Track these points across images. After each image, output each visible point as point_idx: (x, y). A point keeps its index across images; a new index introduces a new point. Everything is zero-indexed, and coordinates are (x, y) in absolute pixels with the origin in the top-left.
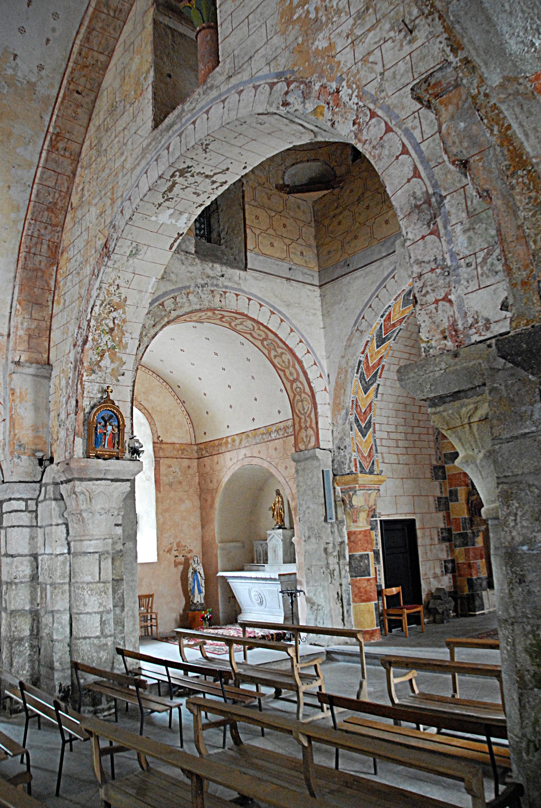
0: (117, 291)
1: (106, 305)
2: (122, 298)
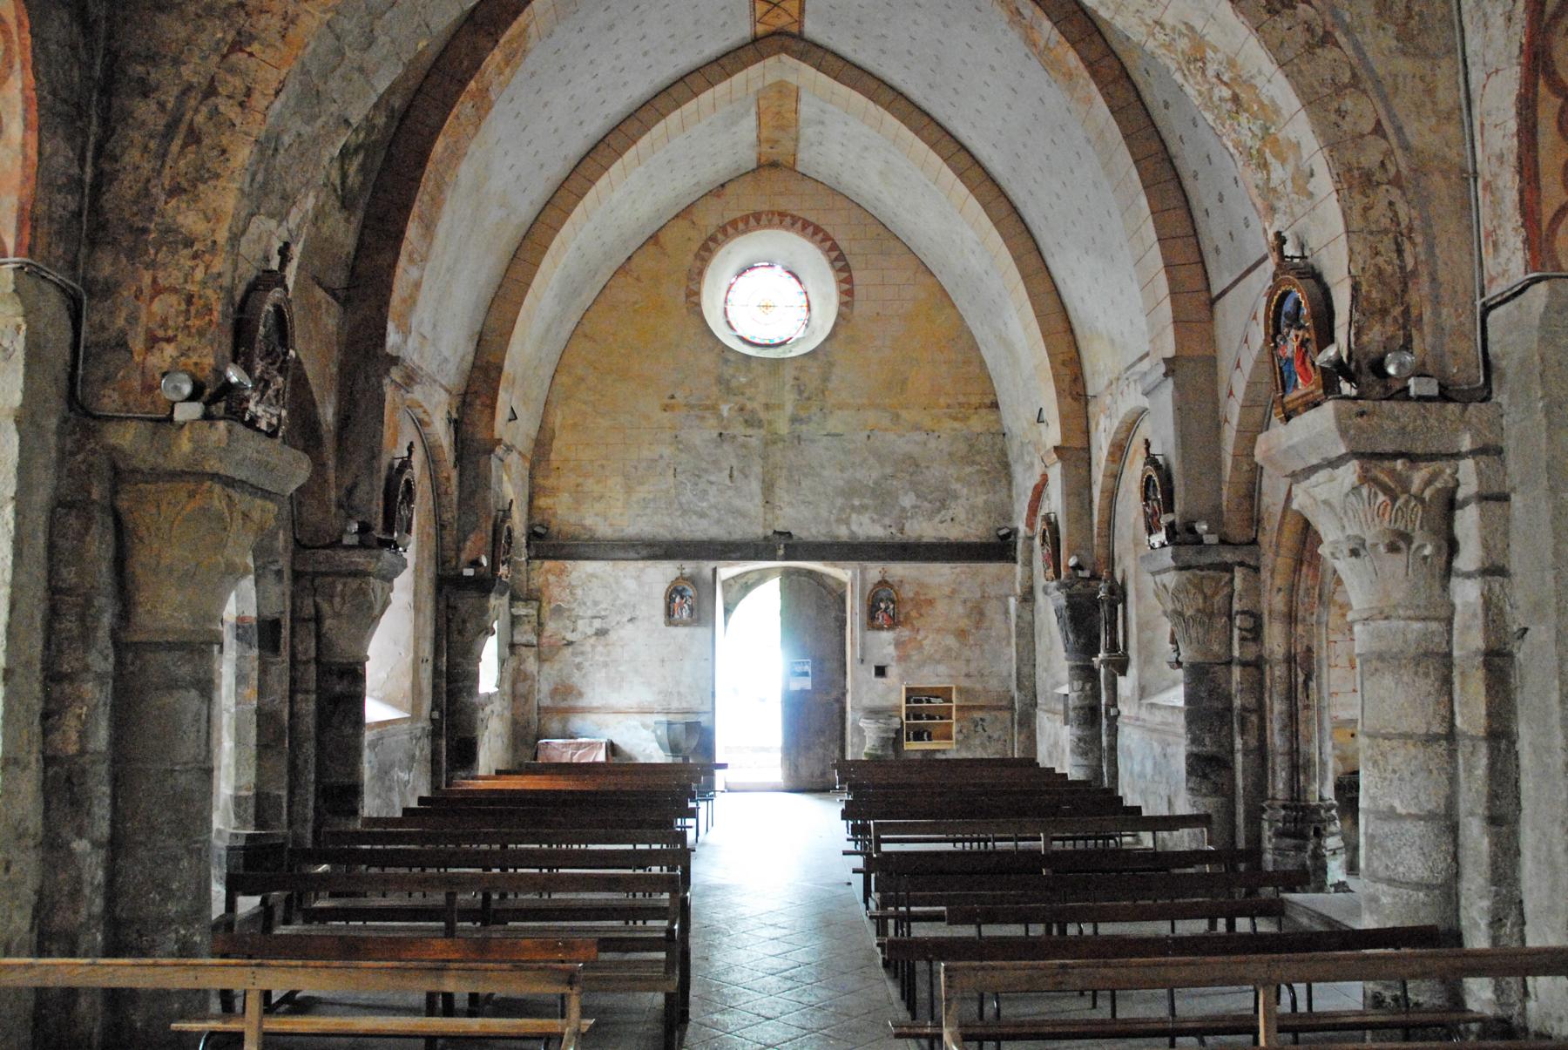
0: (1168, 31)
1: (1189, 70)
2: (1185, 31)
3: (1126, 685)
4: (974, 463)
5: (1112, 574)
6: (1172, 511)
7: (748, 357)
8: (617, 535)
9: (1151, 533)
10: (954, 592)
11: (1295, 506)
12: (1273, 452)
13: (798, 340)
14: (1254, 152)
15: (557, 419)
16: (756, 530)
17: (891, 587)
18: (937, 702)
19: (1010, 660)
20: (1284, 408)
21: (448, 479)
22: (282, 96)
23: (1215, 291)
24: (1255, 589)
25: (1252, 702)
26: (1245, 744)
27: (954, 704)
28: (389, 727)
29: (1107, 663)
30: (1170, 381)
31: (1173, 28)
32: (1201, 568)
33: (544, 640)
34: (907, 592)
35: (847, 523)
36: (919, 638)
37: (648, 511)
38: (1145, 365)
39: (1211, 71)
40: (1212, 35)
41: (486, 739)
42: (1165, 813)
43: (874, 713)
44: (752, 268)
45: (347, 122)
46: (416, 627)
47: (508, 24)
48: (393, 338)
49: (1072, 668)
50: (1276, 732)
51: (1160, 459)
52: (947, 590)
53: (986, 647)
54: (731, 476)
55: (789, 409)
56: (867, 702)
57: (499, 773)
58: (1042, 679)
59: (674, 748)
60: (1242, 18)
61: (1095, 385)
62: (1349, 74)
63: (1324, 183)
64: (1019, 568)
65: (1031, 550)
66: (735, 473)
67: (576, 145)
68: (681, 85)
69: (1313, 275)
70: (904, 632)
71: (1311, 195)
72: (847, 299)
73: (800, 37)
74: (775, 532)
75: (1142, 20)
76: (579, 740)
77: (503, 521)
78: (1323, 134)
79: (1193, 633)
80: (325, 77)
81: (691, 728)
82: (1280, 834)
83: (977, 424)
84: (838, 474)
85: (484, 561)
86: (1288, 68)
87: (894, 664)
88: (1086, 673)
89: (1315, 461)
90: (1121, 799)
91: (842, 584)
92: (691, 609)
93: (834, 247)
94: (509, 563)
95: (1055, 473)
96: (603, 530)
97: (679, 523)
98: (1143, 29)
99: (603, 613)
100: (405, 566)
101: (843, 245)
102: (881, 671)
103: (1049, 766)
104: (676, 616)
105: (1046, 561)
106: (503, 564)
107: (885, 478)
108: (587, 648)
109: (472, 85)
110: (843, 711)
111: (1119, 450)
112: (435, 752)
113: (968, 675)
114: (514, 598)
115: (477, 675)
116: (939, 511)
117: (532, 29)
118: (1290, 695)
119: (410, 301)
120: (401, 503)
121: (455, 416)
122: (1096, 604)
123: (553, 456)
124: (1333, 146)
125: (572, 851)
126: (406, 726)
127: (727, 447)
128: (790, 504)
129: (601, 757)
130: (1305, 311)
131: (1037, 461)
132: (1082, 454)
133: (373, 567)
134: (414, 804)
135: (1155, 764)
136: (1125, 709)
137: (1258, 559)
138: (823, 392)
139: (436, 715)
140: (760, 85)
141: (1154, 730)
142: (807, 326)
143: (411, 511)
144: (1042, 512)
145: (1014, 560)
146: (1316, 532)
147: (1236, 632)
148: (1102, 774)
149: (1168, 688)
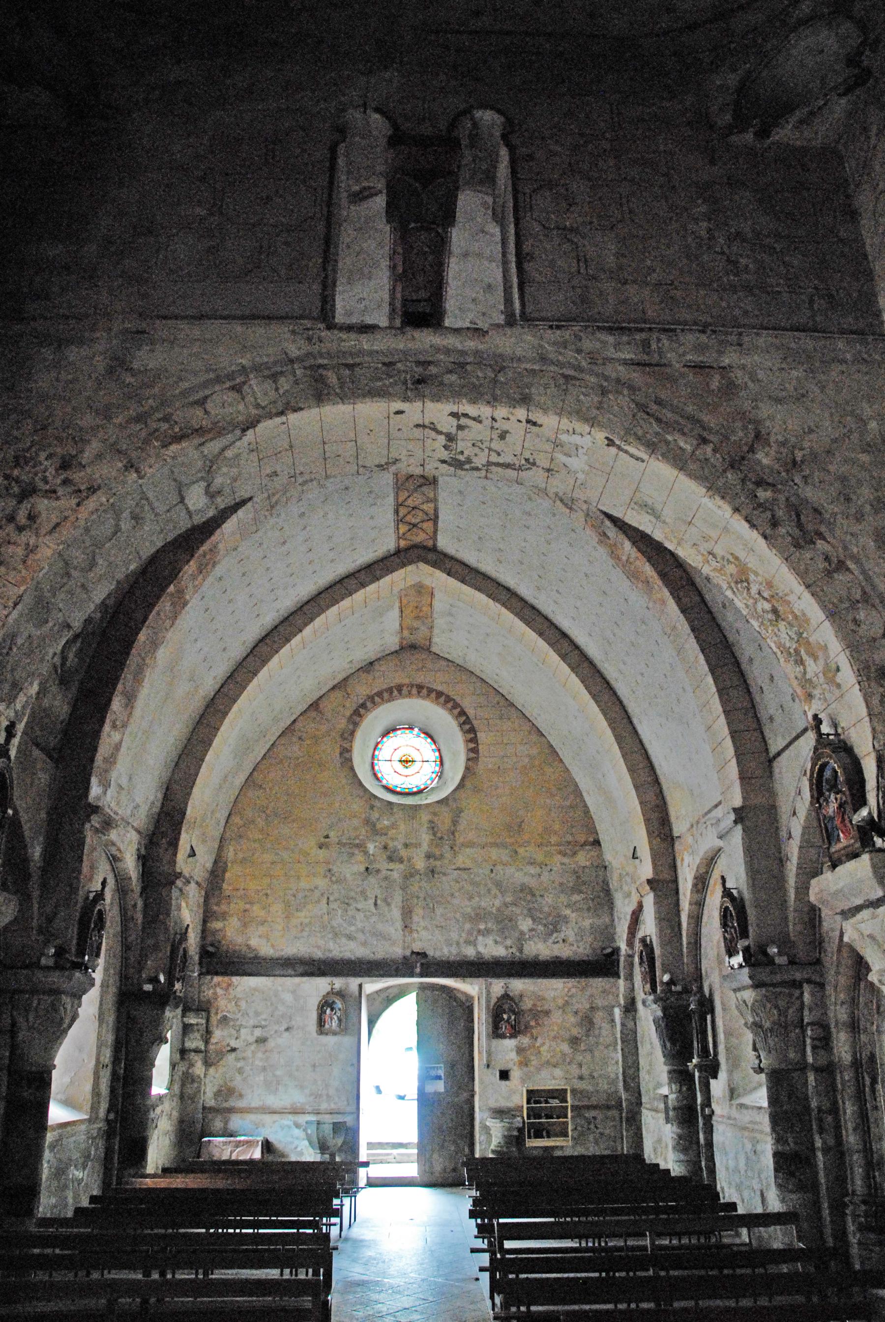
3: (718, 1087)
4: (581, 892)
5: (701, 988)
6: (747, 937)
7: (390, 803)
8: (277, 955)
9: (730, 956)
10: (567, 1003)
11: (846, 939)
12: (825, 893)
13: (433, 789)
14: (792, 651)
15: (230, 853)
16: (397, 951)
17: (512, 999)
18: (555, 1103)
19: (617, 1063)
20: (830, 857)
21: (135, 906)
22: (19, 607)
23: (773, 750)
24: (821, 1004)
25: (826, 1105)
26: (824, 1143)
27: (569, 1104)
28: (69, 1129)
29: (699, 1067)
30: (739, 827)
31: (723, 558)
32: (774, 985)
33: (211, 1047)
34: (527, 1004)
35: (474, 944)
36: (538, 1044)
37: (305, 934)
38: (719, 812)
39: (754, 590)
40: (752, 563)
41: (155, 1137)
42: (759, 1210)
43: (500, 1113)
44: (395, 730)
45: (69, 627)
46: (99, 1035)
47: (202, 542)
48: (95, 790)
49: (670, 1072)
50: (850, 1131)
51: (735, 892)
52: (560, 1002)
53: (597, 1054)
54: (376, 904)
55: (425, 847)
56: (493, 1104)
57: (166, 1171)
58: (645, 1080)
59: (323, 1147)
60: (774, 551)
61: (679, 827)
62: (859, 591)
63: (848, 676)
64: (621, 982)
65: (632, 965)
66: (379, 902)
67: (253, 632)
68: (339, 586)
69: (844, 749)
70: (525, 1040)
71: (839, 686)
72: (472, 755)
73: (434, 549)
74: (413, 953)
75: (699, 552)
76: (238, 1138)
77: (180, 943)
78: (844, 639)
79: (771, 1042)
80: (54, 592)
81: (337, 1127)
82: (861, 1228)
83: (583, 858)
84: (468, 903)
85: (162, 978)
86: (813, 588)
87: (515, 1068)
88: (682, 1077)
89: (859, 902)
90: (717, 1195)
91: (470, 998)
92: (340, 1020)
93: (463, 713)
94: (183, 980)
95: (649, 901)
96: (266, 950)
97: (331, 945)
98: (700, 558)
99: (263, 1023)
100: (93, 985)
101: (471, 712)
102: (504, 1075)
103: (654, 1162)
104: (327, 1026)
105: (644, 979)
106: (178, 980)
107: (506, 905)
108: (249, 1054)
109: (172, 588)
110: (472, 1109)
111: (701, 883)
112: (109, 1151)
113: (581, 1078)
114: (186, 1010)
115: (151, 1078)
116: (551, 934)
117: (220, 546)
118: (860, 1097)
119: (111, 760)
120: (93, 930)
121: (143, 852)
122: (689, 1016)
123: (225, 886)
124: (853, 647)
125: (227, 1233)
126: (83, 1127)
127: (372, 880)
128: (425, 928)
129: (257, 1154)
130: (841, 779)
131: (634, 891)
132: (673, 886)
133: (65, 986)
134: (85, 1203)
135: (747, 1158)
136: (719, 1108)
137: (822, 976)
138: (453, 833)
139: (112, 1116)
140: (402, 587)
141: (744, 1128)
142: (440, 778)
143: (101, 937)
144: (640, 935)
145: (619, 977)
146: (866, 963)
147: (808, 1041)
148: (701, 1169)
149: (755, 1089)
